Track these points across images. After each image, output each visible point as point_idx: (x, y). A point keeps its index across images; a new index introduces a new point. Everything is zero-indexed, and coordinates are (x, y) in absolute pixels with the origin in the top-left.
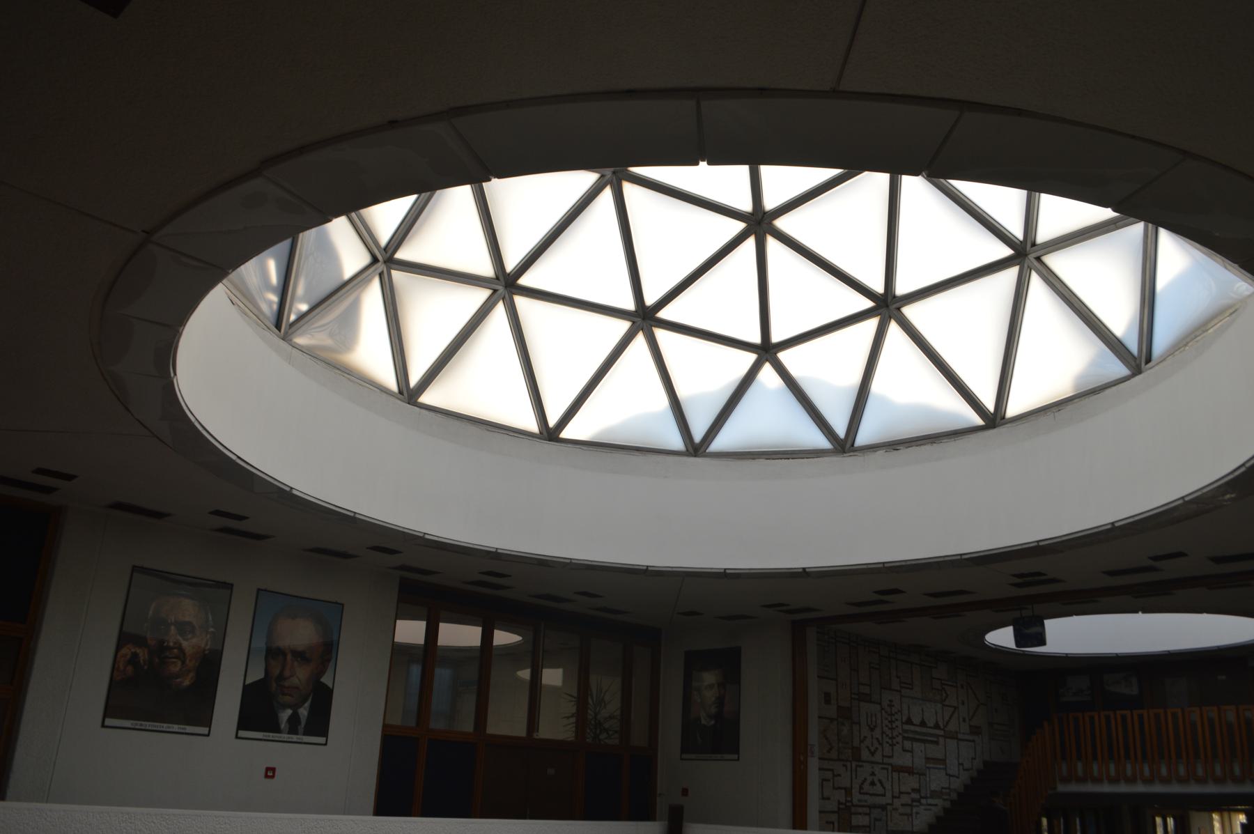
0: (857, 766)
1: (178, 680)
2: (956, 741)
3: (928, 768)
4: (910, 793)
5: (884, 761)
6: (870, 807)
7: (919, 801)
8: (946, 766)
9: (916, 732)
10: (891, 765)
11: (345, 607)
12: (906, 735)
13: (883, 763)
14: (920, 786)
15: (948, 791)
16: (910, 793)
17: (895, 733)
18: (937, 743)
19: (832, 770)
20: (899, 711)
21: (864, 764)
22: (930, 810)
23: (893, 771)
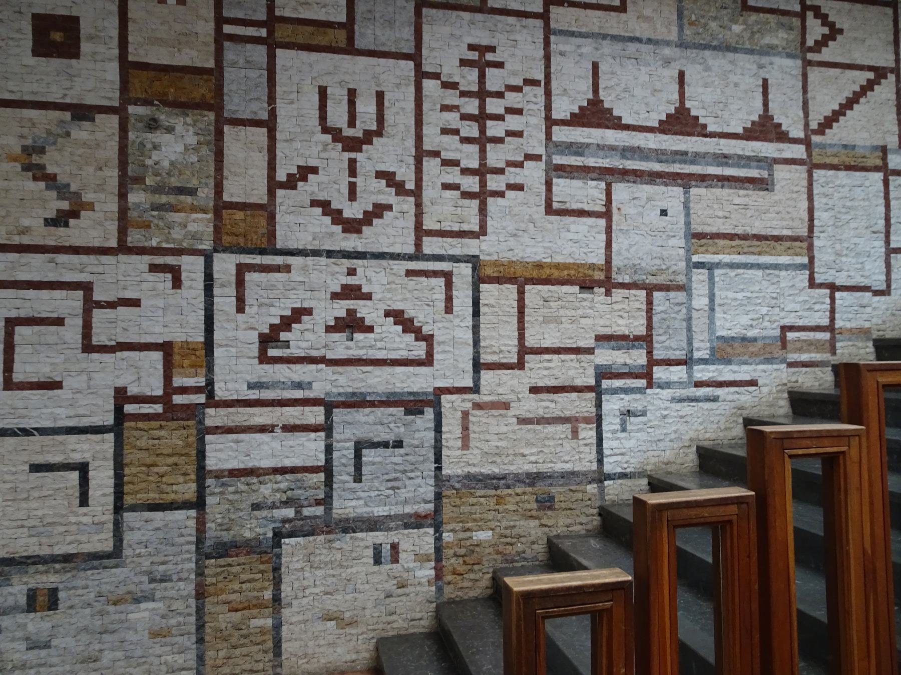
0: (242, 270)
1: (212, 102)
2: (879, 176)
3: (700, 265)
4: (590, 351)
5: (427, 250)
6: (329, 406)
7: (647, 374)
8: (812, 259)
9: (723, 159)
10: (474, 261)
11: (91, 474)
12: (558, 160)
13: (418, 257)
14: (650, 326)
15: (826, 336)
16: (590, 351)
17: (496, 156)
18: (763, 184)
19: (86, 288)
20: (534, 83)
21: (290, 260)
22: (715, 399)
23: (478, 280)
